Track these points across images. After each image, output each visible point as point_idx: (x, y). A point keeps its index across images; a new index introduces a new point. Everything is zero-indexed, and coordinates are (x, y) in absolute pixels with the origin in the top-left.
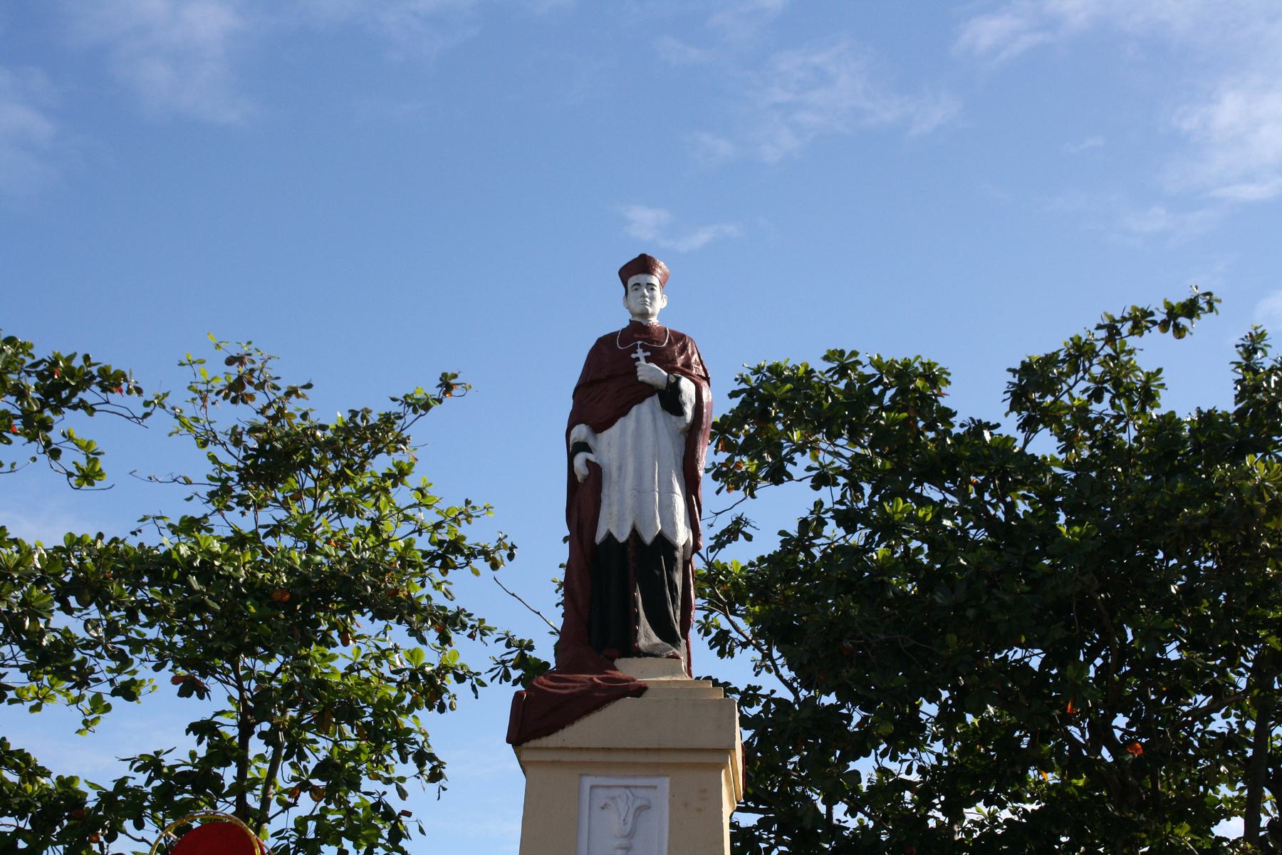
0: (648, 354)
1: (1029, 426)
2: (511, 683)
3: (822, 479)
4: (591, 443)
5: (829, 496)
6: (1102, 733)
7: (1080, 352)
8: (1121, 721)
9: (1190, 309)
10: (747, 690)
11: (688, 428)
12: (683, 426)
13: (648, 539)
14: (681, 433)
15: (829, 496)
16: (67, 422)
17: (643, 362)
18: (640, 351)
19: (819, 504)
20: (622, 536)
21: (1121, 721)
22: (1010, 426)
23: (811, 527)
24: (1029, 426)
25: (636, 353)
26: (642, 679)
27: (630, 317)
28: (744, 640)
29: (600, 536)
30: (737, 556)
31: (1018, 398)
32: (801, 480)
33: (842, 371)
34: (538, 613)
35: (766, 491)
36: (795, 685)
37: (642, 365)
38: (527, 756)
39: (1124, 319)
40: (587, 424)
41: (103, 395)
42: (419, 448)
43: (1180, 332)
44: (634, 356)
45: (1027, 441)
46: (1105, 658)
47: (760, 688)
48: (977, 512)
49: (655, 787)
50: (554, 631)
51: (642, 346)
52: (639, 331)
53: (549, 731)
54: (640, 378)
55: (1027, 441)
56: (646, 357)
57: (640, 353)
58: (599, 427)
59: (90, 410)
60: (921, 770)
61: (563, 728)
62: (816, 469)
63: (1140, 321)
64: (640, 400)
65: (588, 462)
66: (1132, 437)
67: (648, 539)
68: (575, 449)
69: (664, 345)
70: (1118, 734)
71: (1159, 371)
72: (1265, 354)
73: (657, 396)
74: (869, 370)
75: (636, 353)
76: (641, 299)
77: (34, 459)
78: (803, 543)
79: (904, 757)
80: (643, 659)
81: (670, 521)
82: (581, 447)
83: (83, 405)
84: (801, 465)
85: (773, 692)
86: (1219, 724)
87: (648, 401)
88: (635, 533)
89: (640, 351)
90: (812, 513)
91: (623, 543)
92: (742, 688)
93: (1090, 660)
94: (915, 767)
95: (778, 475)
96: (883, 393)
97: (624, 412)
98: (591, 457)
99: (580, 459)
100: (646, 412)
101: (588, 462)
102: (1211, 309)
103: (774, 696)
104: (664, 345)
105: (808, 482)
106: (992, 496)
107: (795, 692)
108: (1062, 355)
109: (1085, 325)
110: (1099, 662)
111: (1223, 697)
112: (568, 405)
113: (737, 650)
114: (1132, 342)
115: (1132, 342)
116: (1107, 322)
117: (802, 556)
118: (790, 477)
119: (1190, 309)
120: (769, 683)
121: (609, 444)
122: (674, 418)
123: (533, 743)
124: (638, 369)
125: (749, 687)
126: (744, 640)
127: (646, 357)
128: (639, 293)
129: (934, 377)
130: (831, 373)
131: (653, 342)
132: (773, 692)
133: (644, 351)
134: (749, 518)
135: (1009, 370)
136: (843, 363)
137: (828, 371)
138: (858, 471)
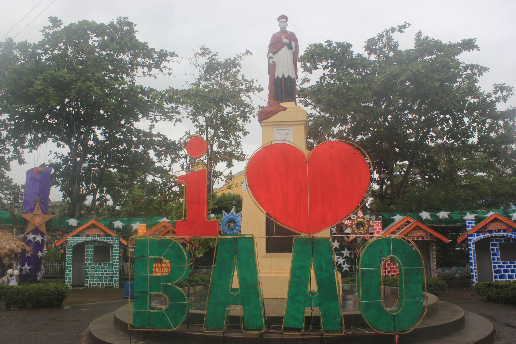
1: (370, 54)
3: (325, 68)
4: (273, 57)
5: (327, 72)
6: (386, 119)
7: (381, 37)
8: (389, 116)
9: (404, 27)
13: (286, 77)
15: (327, 72)
16: (164, 64)
17: (283, 38)
18: (283, 36)
20: (280, 77)
21: (389, 116)
22: (365, 55)
23: (323, 78)
24: (370, 54)
26: (286, 106)
27: (280, 29)
29: (276, 77)
30: (306, 86)
31: (367, 48)
33: (330, 45)
35: (314, 72)
38: (262, 124)
39: (390, 30)
41: (171, 58)
43: (402, 32)
45: (369, 57)
46: (386, 103)
48: (359, 74)
49: (290, 129)
52: (283, 31)
53: (267, 118)
55: (369, 57)
57: (283, 37)
58: (275, 53)
59: (168, 61)
60: (348, 128)
61: (269, 118)
63: (393, 30)
64: (283, 47)
65: (272, 61)
66: (392, 55)
67: (286, 77)
68: (270, 58)
70: (389, 120)
71: (398, 41)
72: (422, 37)
74: (335, 45)
77: (158, 74)
79: (344, 126)
82: (271, 58)
83: (166, 60)
84: (320, 66)
85: (316, 114)
86: (410, 117)
87: (285, 47)
88: (283, 76)
89: (283, 36)
93: (383, 104)
94: (346, 128)
95: (316, 68)
96: (338, 49)
97: (280, 49)
98: (273, 60)
99: (271, 60)
100: (285, 49)
101: (272, 61)
102: (409, 26)
106: (362, 70)
107: (320, 113)
108: (376, 38)
109: (381, 30)
110: (385, 104)
111: (411, 111)
112: (267, 49)
114: (392, 34)
115: (392, 34)
116: (386, 30)
118: (318, 68)
119: (404, 27)
120: (314, 112)
122: (291, 50)
123: (263, 121)
128: (282, 23)
129: (349, 46)
132: (316, 114)
135: (365, 42)
136: (329, 43)
138: (333, 66)
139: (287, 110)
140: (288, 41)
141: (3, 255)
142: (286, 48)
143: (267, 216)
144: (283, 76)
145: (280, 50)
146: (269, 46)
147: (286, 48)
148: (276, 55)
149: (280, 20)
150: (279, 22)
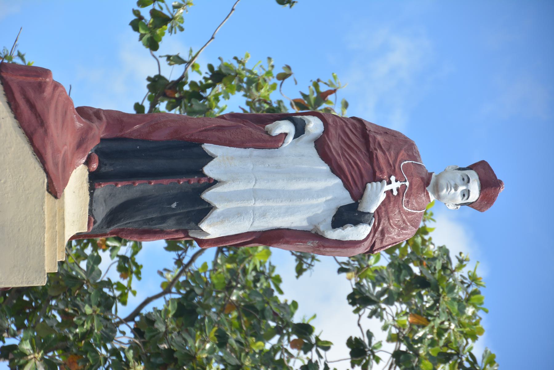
0: (395, 193)
2: (136, 8)
4: (304, 138)
10: (136, 265)
11: (320, 234)
12: (321, 228)
13: (207, 196)
14: (315, 226)
17: (387, 188)
18: (399, 184)
19: (326, 346)
20: (209, 170)
25: (396, 181)
28: (186, 261)
29: (209, 148)
32: (359, 325)
34: (213, 38)
36: (137, 319)
37: (382, 186)
40: (323, 132)
42: (235, 7)
44: (393, 178)
47: (139, 279)
50: (194, 54)
51: (404, 187)
54: (369, 185)
56: (392, 191)
57: (395, 185)
62: (370, 342)
64: (347, 186)
67: (207, 196)
69: (405, 208)
73: (353, 202)
75: (396, 181)
76: (453, 183)
78: (284, 328)
80: (88, 193)
81: (226, 217)
85: (134, 293)
87: (347, 194)
88: (212, 183)
89: (399, 184)
90: (317, 339)
91: (202, 171)
92: (139, 259)
97: (337, 170)
101: (286, 134)
103: (130, 294)
104: (405, 208)
105: (357, 334)
113: (173, 255)
117: (273, 324)
121: (303, 155)
122: (330, 220)
124: (379, 183)
125: (138, 267)
126: (186, 261)
127: (392, 191)
128: (459, 181)
130: (470, 359)
131: (408, 196)
133: (398, 189)
134: (314, 268)
137: (472, 355)
139: (48, 198)
140: (373, 210)
141: (420, 330)
142: (346, 198)
143: (376, 213)
144: (212, 183)
145: (333, 171)
146: (360, 121)
147: (346, 198)
148: (314, 152)
149: (473, 176)
150: (470, 168)
